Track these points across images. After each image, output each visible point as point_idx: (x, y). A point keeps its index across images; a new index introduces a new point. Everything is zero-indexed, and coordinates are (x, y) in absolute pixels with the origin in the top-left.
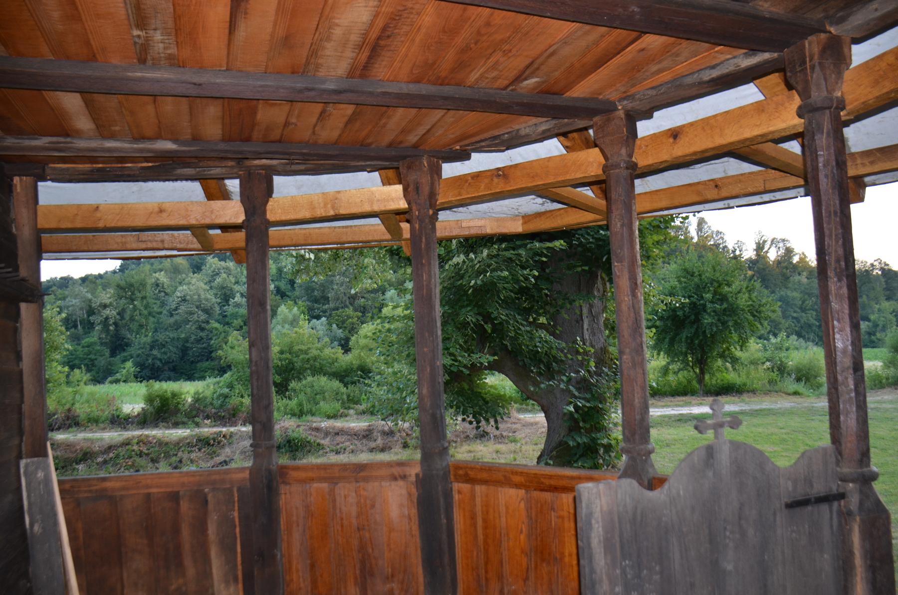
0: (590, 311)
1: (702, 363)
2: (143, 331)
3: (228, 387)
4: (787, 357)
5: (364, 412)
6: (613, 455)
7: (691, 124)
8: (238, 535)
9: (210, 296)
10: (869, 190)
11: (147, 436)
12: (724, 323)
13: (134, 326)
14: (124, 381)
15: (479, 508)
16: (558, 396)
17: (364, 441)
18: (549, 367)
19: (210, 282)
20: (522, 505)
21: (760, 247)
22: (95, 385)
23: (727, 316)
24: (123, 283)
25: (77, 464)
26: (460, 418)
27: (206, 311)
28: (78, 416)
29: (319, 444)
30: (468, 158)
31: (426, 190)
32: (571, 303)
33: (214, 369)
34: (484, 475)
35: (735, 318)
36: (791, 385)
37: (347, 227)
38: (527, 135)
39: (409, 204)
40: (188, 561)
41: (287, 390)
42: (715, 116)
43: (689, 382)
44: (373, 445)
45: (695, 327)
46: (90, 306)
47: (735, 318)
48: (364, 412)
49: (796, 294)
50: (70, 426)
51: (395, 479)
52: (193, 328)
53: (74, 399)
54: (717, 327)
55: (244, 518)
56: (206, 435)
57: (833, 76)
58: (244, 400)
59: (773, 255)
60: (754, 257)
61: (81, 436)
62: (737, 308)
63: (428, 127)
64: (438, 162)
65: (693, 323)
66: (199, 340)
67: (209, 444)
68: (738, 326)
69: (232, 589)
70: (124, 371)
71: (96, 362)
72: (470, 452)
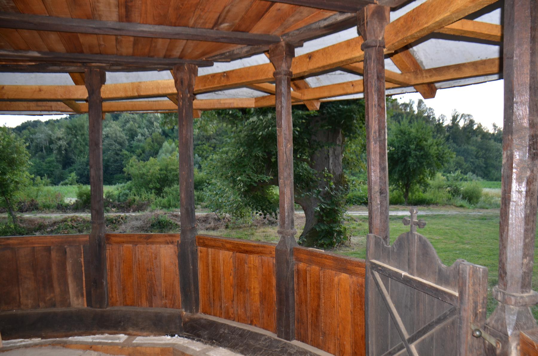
0: (334, 153)
1: (407, 186)
2: (82, 155)
3: (128, 190)
4: (461, 185)
5: (206, 207)
6: (342, 237)
7: (317, 51)
8: (83, 271)
9: (123, 135)
10: (438, 91)
11: (77, 217)
12: (421, 163)
13: (77, 151)
14: (71, 184)
15: (210, 261)
16: (313, 201)
17: (203, 224)
18: (307, 184)
19: (123, 126)
20: (231, 260)
21: (454, 119)
22: (52, 186)
23: (423, 159)
24: (70, 125)
25: (35, 232)
26: (255, 212)
27: (120, 144)
28: (38, 204)
29: (177, 225)
30: (212, 65)
31: (186, 83)
32: (321, 147)
33: (124, 179)
34: (212, 243)
35: (428, 160)
36: (459, 201)
37: (155, 101)
38: (238, 54)
39: (177, 90)
40: (56, 285)
41: (162, 192)
42: (328, 47)
43: (399, 197)
44: (208, 226)
45: (404, 164)
46: (51, 139)
47: (428, 160)
48: (206, 207)
49: (473, 148)
50: (33, 210)
51: (168, 243)
52: (112, 154)
53: (37, 194)
54: (417, 165)
55: (87, 262)
56: (111, 217)
57: (379, 28)
58: (136, 198)
59: (462, 124)
60: (450, 125)
61: (39, 215)
62: (429, 154)
63: (182, 48)
64: (195, 67)
65: (403, 162)
66: (116, 161)
67: (113, 223)
68: (429, 165)
69: (80, 300)
70: (70, 178)
71: (54, 172)
72: (264, 232)
